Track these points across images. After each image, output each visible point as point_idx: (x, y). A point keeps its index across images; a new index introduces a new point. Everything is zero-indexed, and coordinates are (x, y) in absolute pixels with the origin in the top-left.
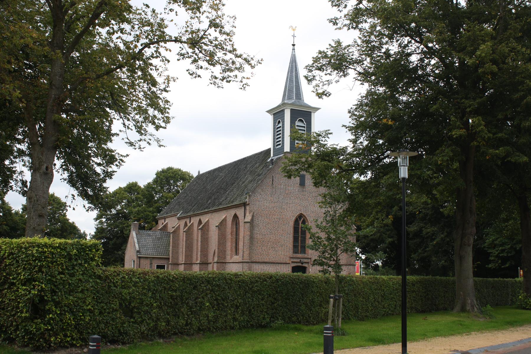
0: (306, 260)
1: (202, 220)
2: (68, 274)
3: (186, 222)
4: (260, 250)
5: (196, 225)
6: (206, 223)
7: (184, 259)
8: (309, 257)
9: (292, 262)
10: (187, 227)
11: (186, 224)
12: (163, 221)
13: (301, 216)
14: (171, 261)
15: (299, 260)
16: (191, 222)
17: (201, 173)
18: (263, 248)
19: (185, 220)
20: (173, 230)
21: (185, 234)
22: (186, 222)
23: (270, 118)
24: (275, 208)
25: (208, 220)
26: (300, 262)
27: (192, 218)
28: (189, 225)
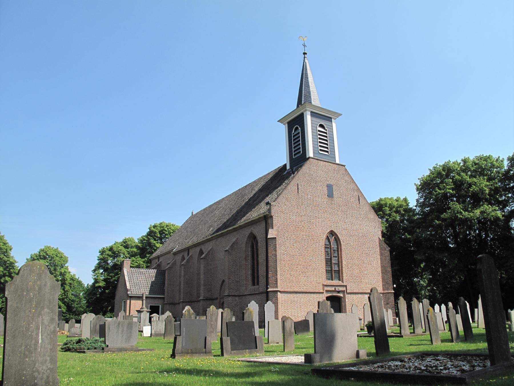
0: (341, 289)
1: (204, 250)
2: (405, 362)
3: (183, 256)
4: (288, 276)
5: (196, 257)
6: (209, 252)
7: (182, 297)
8: (344, 284)
9: (326, 291)
10: (185, 261)
11: (183, 258)
12: (157, 260)
13: (332, 233)
14: (166, 300)
15: (333, 289)
16: (190, 255)
17: (194, 213)
18: (292, 273)
19: (182, 254)
20: (169, 266)
21: (183, 267)
22: (183, 256)
23: (283, 129)
24: (303, 223)
25: (212, 248)
26: (335, 291)
27: (190, 250)
28: (187, 258)
